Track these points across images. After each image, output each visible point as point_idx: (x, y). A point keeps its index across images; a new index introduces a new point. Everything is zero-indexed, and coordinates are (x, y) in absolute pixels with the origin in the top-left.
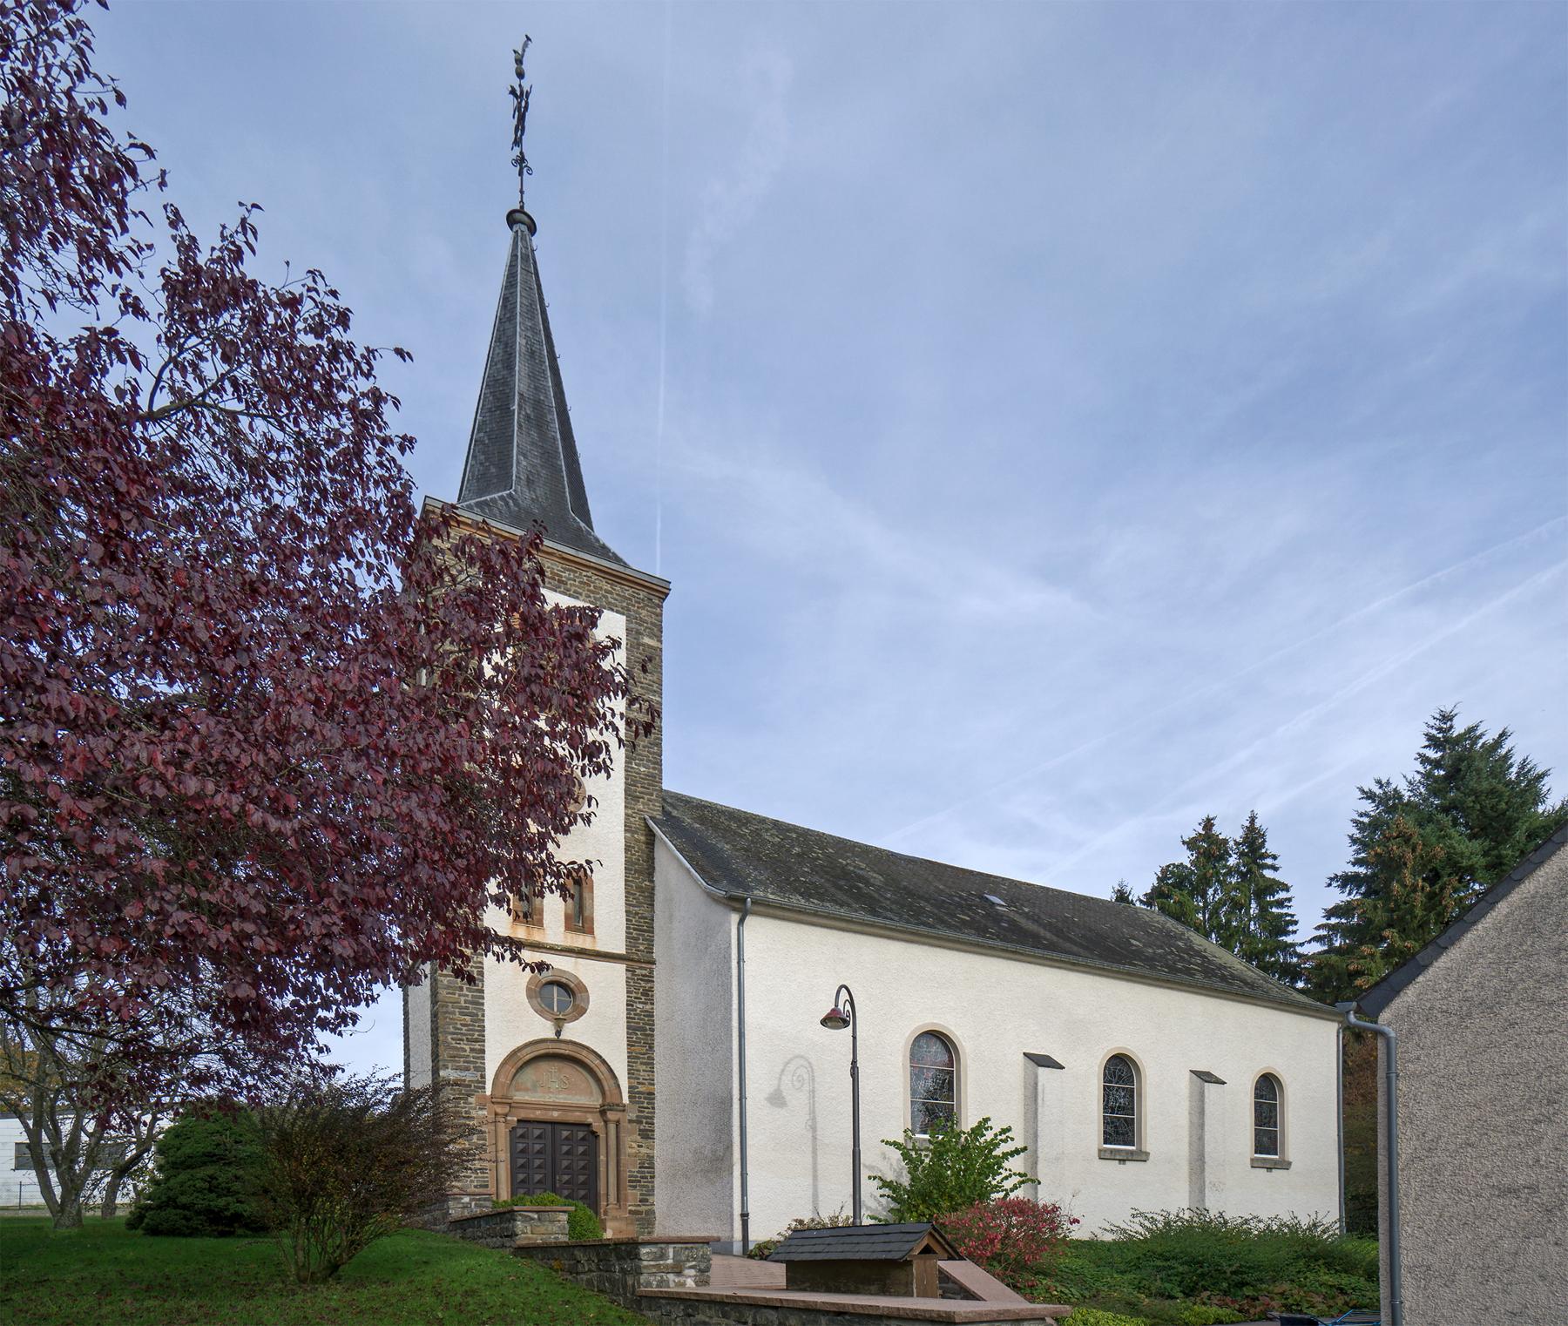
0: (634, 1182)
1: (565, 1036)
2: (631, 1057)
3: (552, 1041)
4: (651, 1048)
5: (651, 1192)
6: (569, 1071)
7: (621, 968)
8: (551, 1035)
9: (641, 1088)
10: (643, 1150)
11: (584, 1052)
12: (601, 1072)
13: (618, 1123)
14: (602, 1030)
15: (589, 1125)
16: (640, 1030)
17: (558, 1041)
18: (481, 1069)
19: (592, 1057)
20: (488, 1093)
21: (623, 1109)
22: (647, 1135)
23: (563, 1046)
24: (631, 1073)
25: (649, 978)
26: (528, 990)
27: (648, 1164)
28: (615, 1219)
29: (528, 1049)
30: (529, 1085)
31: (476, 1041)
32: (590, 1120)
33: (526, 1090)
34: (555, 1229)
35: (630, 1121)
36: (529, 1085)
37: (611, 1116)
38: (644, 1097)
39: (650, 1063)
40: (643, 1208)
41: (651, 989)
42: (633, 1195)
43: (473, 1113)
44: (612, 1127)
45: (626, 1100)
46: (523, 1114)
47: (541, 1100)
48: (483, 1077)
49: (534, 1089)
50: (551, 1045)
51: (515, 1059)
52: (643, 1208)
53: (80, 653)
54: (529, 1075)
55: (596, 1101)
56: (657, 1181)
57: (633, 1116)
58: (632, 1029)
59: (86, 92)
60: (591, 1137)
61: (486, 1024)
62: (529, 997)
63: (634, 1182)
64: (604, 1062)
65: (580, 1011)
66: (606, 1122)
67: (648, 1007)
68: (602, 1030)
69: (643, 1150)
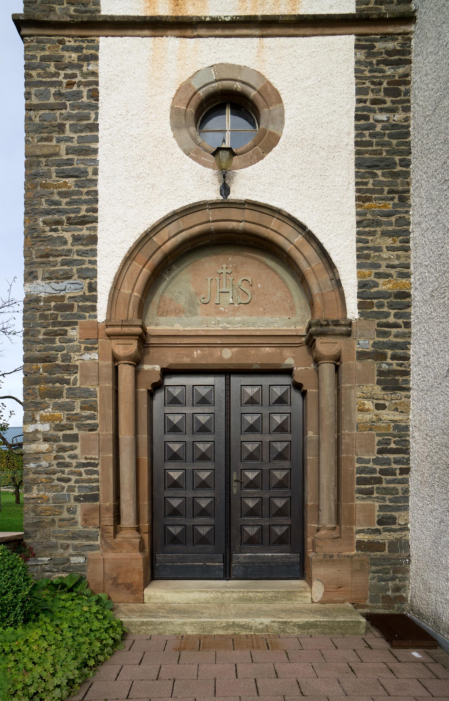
0: (369, 483)
1: (236, 194)
2: (365, 224)
3: (214, 205)
4: (404, 198)
5: (401, 501)
6: (252, 270)
7: (342, 47)
8: (213, 194)
9: (384, 286)
10: (387, 415)
11: (274, 223)
12: (305, 257)
13: (337, 360)
14: (307, 176)
15: (289, 372)
16: (383, 163)
17: (225, 203)
18: (90, 274)
19: (287, 230)
20: (101, 315)
21: (347, 330)
22: (395, 382)
23: (234, 213)
24: (364, 255)
25: (402, 57)
26: (175, 112)
27: (396, 444)
28: (329, 559)
29: (172, 228)
30: (182, 302)
31: (83, 221)
32: (289, 361)
33: (178, 312)
34: (237, 629)
35: (362, 355)
36: (182, 302)
37: (324, 346)
38: (389, 304)
39: (402, 233)
40: (386, 537)
41: (405, 80)
42: (364, 509)
43: (76, 359)
44: (327, 369)
45: (353, 312)
46: (172, 357)
47: (201, 329)
48: (93, 288)
49: (191, 308)
50: (211, 214)
51: (147, 249)
52: (386, 537)
53: (195, 353)
54: (183, 284)
55: (295, 323)
56: (414, 479)
57: (365, 343)
58: (365, 165)
59: (132, 580)
60: (296, 396)
61: (101, 188)
62: (176, 126)
63: (369, 483)
64: (310, 237)
65: (267, 142)
66: (316, 361)
67: (398, 117)
68: (307, 176)
69: (387, 415)
